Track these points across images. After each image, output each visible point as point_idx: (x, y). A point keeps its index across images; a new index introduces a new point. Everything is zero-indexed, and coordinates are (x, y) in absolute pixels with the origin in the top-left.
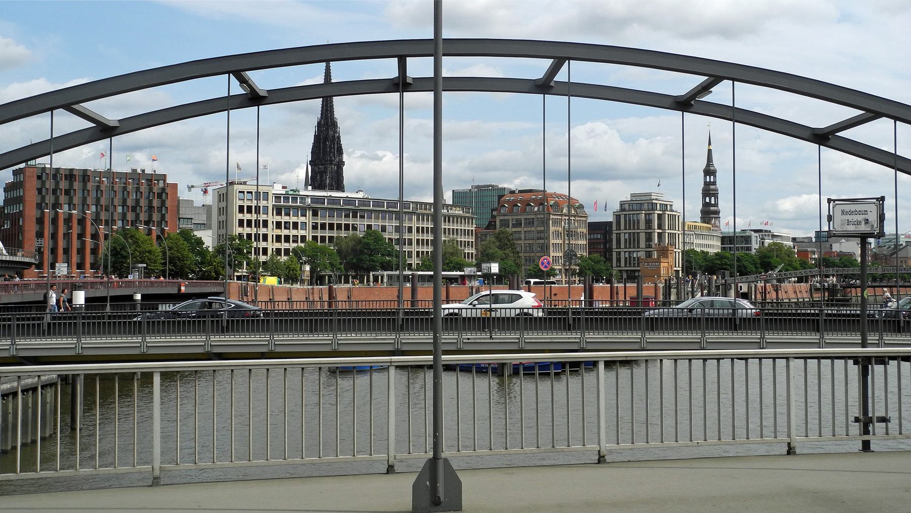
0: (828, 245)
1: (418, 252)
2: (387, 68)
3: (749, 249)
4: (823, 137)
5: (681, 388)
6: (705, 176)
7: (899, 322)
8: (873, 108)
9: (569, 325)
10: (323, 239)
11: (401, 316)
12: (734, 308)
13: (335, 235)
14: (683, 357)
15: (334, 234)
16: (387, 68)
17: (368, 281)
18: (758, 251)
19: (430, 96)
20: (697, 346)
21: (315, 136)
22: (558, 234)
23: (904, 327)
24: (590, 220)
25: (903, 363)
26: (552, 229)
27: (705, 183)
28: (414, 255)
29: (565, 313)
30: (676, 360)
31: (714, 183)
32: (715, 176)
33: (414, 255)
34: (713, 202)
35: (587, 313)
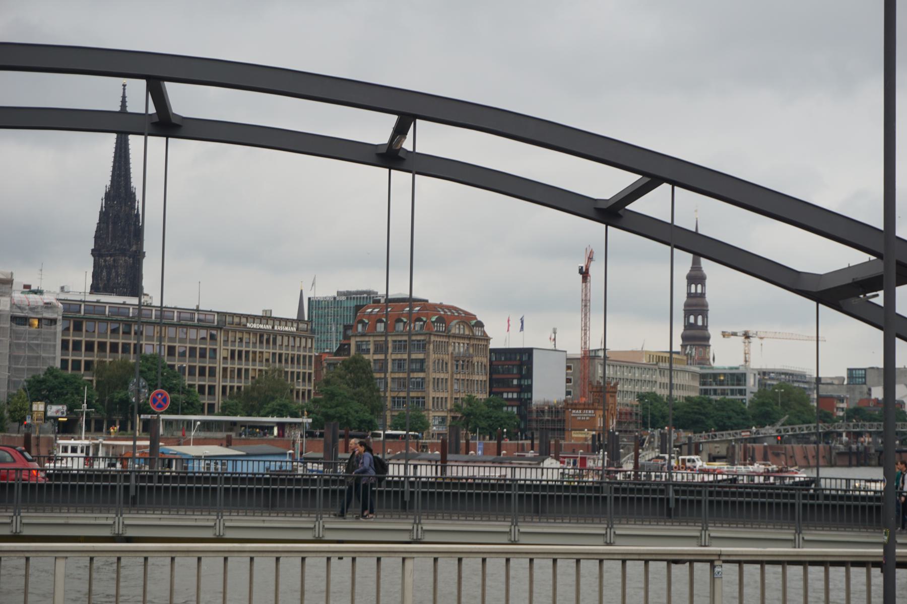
0: (865, 388)
1: (224, 388)
2: (376, 128)
3: (742, 392)
4: (612, 213)
5: (778, 599)
6: (689, 285)
7: (668, 500)
8: (655, 170)
9: (404, 503)
10: (76, 364)
11: (671, 494)
12: (294, 469)
13: (96, 359)
14: (589, 555)
15: (95, 358)
16: (376, 128)
17: (133, 428)
18: (759, 395)
19: (111, 139)
20: (505, 539)
21: (101, 212)
22: (442, 365)
23: (134, 498)
24: (493, 345)
25: (853, 570)
26: (433, 356)
27: (690, 295)
28: (218, 391)
29: (662, 491)
30: (601, 561)
31: (703, 295)
32: (703, 285)
33: (218, 391)
34: (700, 323)
35: (326, 482)
